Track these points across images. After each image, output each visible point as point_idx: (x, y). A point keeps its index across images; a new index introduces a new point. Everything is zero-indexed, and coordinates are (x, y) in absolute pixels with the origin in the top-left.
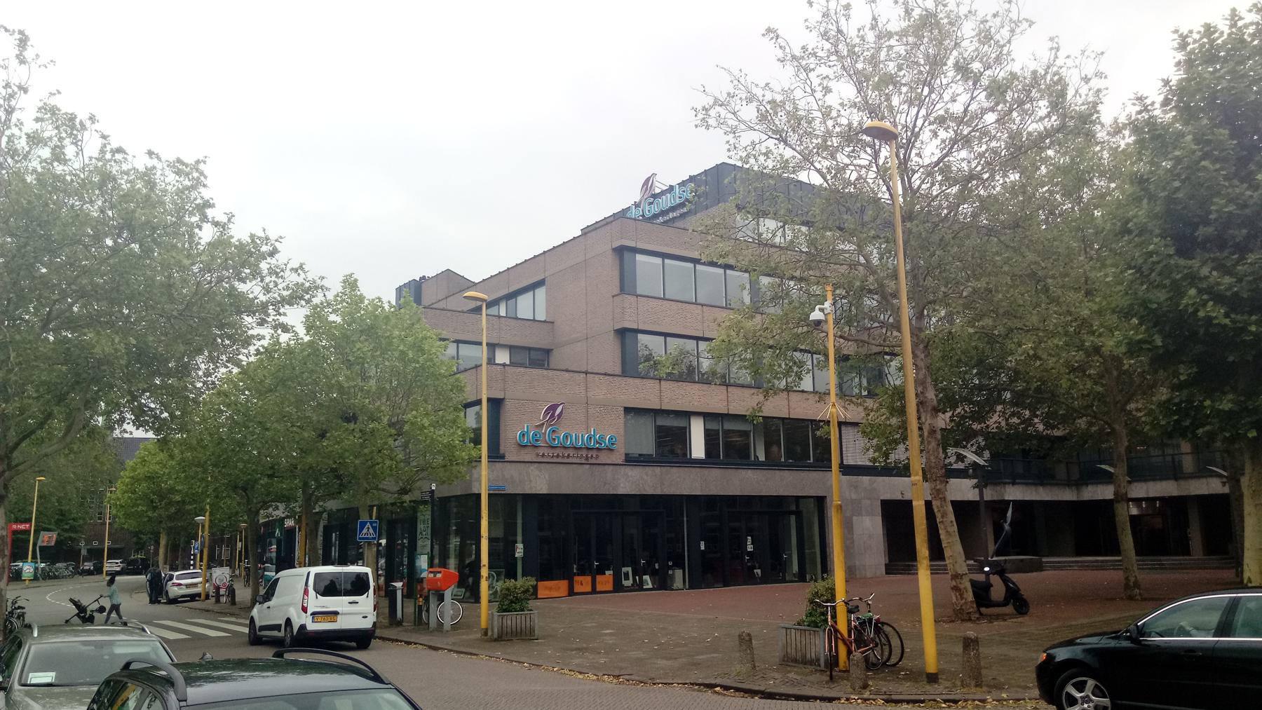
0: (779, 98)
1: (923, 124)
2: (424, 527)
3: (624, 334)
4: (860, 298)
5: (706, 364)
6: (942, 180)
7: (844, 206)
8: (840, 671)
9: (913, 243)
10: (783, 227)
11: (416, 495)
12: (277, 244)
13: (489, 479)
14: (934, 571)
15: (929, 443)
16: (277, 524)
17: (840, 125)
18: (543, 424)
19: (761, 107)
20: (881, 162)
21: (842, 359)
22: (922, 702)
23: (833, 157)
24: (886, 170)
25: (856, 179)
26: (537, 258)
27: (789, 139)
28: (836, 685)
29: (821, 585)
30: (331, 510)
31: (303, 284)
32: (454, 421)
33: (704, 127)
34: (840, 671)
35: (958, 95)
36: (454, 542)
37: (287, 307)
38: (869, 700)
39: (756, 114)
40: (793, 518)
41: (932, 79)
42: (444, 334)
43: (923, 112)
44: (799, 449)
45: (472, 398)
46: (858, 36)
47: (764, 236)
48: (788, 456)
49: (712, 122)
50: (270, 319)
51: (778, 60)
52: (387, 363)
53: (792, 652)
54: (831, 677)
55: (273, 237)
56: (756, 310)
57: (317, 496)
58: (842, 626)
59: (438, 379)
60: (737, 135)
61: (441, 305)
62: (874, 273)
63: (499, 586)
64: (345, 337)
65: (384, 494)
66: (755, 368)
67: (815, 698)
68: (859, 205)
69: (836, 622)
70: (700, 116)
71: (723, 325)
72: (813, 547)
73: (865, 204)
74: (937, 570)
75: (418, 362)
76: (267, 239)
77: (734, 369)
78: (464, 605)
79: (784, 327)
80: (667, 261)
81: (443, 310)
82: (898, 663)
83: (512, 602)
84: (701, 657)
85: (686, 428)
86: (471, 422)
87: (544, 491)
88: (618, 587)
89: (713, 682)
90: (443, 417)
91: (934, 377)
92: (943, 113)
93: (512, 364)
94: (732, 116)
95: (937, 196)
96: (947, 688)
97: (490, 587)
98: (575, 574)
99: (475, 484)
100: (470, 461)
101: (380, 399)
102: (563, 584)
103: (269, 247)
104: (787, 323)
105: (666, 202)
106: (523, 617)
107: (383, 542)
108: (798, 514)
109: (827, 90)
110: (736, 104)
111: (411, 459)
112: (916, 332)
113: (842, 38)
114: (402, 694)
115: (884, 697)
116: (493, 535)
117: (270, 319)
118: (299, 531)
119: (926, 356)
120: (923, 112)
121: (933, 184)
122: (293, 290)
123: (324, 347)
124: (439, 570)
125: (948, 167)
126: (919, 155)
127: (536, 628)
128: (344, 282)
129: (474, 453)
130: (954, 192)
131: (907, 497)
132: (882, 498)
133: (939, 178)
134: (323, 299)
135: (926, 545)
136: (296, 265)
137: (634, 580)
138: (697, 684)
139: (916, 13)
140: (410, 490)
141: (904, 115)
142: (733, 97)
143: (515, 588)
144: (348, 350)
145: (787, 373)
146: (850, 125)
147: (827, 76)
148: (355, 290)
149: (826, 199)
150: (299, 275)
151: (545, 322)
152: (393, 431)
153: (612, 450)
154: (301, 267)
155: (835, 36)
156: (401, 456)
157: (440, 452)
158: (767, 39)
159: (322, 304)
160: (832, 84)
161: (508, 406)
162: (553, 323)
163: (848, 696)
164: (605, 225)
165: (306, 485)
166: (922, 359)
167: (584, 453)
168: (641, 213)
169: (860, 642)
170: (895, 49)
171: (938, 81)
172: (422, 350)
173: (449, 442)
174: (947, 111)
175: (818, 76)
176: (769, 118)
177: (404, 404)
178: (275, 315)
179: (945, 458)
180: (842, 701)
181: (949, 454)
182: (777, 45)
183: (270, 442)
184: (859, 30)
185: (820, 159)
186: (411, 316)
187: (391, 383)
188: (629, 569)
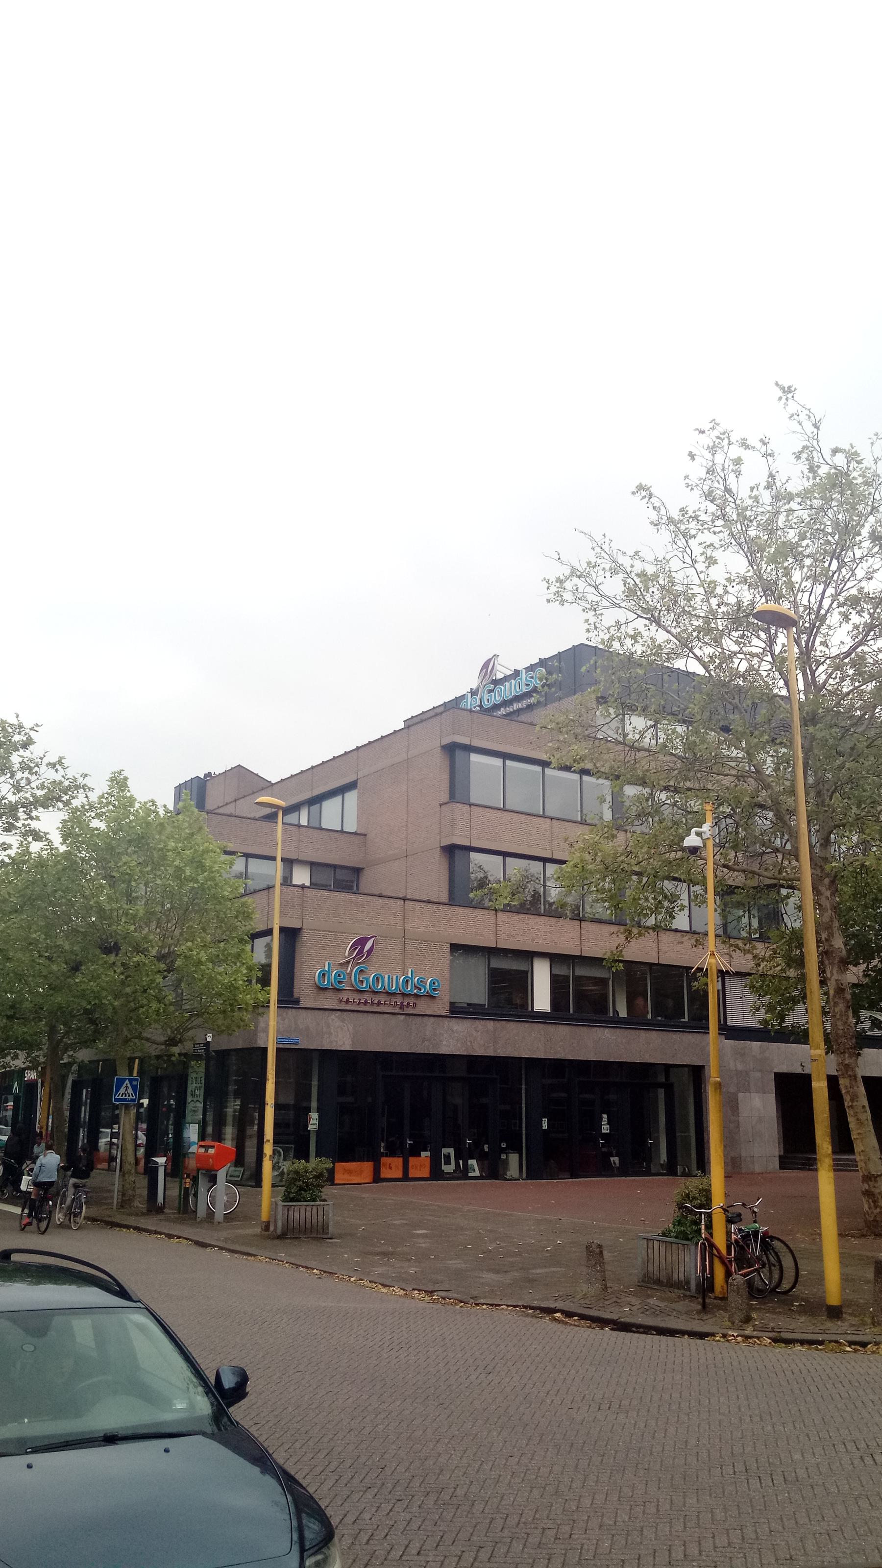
0: (651, 570)
1: (831, 605)
2: (195, 1087)
3: (451, 851)
4: (751, 816)
5: (554, 894)
6: (854, 674)
7: (730, 703)
8: (716, 1298)
9: (816, 751)
10: (655, 726)
11: (188, 1047)
12: (32, 734)
13: (278, 1031)
14: (838, 1167)
15: (836, 1004)
16: (16, 1075)
17: (728, 605)
18: (348, 962)
19: (629, 580)
20: (777, 649)
21: (726, 891)
22: (821, 1343)
23: (717, 641)
24: (784, 660)
25: (746, 671)
26: (350, 755)
27: (662, 619)
28: (709, 1316)
29: (693, 1184)
30: (82, 1061)
31: (61, 783)
32: (238, 956)
33: (558, 602)
34: (716, 1298)
35: (875, 571)
36: (233, 1106)
37: (41, 809)
38: (751, 1337)
39: (623, 588)
40: (661, 1093)
41: (842, 550)
42: (231, 847)
43: (830, 591)
44: (670, 1003)
45: (262, 927)
46: (750, 497)
47: (630, 736)
48: (656, 1010)
49: (568, 596)
50: (19, 824)
51: (652, 523)
52: (159, 882)
53: (653, 1269)
54: (704, 1305)
55: (27, 724)
56: (619, 825)
57: (66, 1043)
58: (720, 1240)
59: (220, 903)
60: (598, 612)
61: (229, 810)
62: (767, 787)
63: (286, 1166)
64: (110, 849)
65: (148, 1044)
66: (615, 900)
67: (682, 1333)
68: (749, 702)
69: (711, 1235)
70: (553, 589)
71: (576, 846)
72: (687, 1129)
73: (757, 701)
74: (849, 1166)
75: (197, 881)
76: (21, 727)
77: (589, 899)
78: (242, 1189)
79: (653, 851)
80: (508, 762)
81: (230, 816)
82: (790, 1290)
83: (301, 1189)
84: (539, 1271)
85: (527, 972)
86: (259, 957)
87: (347, 1047)
88: (436, 1174)
89: (552, 1306)
90: (225, 949)
91: (843, 919)
92: (856, 593)
93: (314, 885)
94: (593, 590)
95: (848, 694)
96: (854, 1325)
97: (275, 1167)
98: (382, 1155)
99: (261, 1035)
100: (256, 1006)
101: (149, 926)
102: (367, 1167)
103: (22, 737)
104: (657, 846)
105: (509, 690)
106: (315, 1208)
107: (145, 1102)
108: (669, 1088)
109: (711, 561)
110: (598, 576)
111: (184, 1002)
112: (817, 863)
113: (731, 499)
114: (151, 1314)
115: (771, 1335)
116: (282, 1100)
117: (19, 824)
118: (42, 1086)
119: (833, 894)
120: (830, 591)
121: (842, 680)
122: (49, 789)
123: (83, 859)
124: (212, 1144)
125: (862, 658)
126: (824, 644)
127: (331, 1223)
128: (112, 780)
129: (261, 997)
130: (869, 688)
131: (806, 1071)
132: (776, 1070)
133: (851, 672)
134: (85, 801)
135: (828, 1139)
136: (54, 760)
137: (457, 1164)
138: (531, 1308)
139: (823, 470)
140: (180, 1041)
141: (807, 594)
142: (594, 567)
143: (306, 1172)
144: (112, 864)
145: (656, 910)
146: (739, 603)
147: (712, 545)
148: (123, 791)
149: (708, 695)
150: (57, 771)
151: (355, 834)
152: (163, 966)
153: (432, 997)
154: (60, 762)
155: (722, 497)
156: (171, 998)
157: (220, 995)
158: (638, 497)
159: (83, 806)
160: (718, 554)
161: (306, 938)
162: (365, 835)
163: (725, 1331)
164: (432, 717)
165: (53, 1030)
166: (827, 898)
167: (399, 1000)
168: (479, 703)
169: (742, 1260)
170: (796, 514)
171: (850, 554)
172: (201, 866)
173: (230, 982)
174: (860, 590)
175: (700, 544)
176: (639, 593)
177: (177, 932)
178: (26, 819)
179: (857, 1023)
180: (718, 1338)
181: (862, 1019)
182: (649, 505)
183: (11, 975)
184: (752, 489)
185: (700, 644)
186: (190, 825)
187: (163, 906)
188: (451, 1151)
